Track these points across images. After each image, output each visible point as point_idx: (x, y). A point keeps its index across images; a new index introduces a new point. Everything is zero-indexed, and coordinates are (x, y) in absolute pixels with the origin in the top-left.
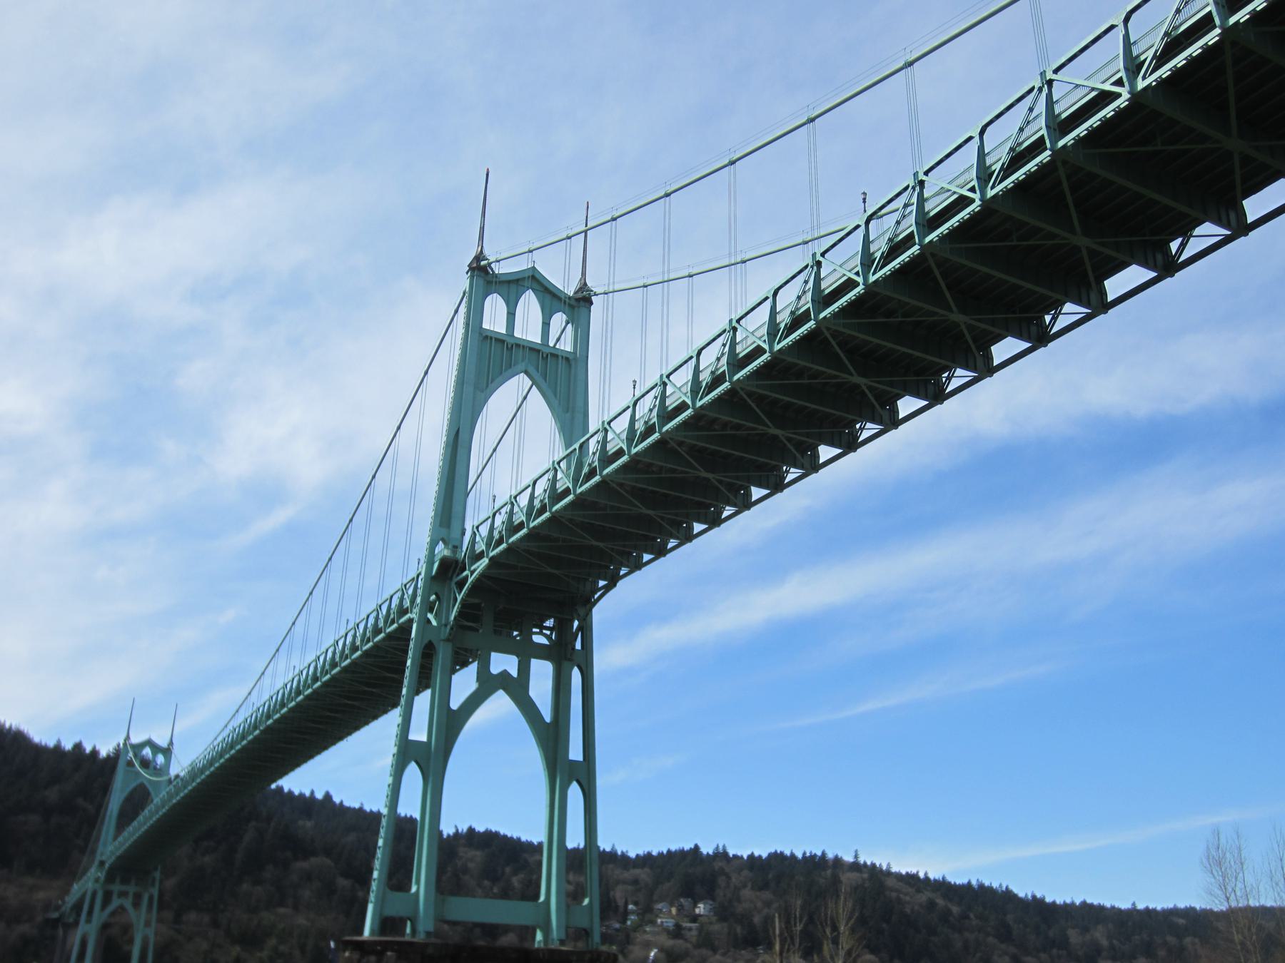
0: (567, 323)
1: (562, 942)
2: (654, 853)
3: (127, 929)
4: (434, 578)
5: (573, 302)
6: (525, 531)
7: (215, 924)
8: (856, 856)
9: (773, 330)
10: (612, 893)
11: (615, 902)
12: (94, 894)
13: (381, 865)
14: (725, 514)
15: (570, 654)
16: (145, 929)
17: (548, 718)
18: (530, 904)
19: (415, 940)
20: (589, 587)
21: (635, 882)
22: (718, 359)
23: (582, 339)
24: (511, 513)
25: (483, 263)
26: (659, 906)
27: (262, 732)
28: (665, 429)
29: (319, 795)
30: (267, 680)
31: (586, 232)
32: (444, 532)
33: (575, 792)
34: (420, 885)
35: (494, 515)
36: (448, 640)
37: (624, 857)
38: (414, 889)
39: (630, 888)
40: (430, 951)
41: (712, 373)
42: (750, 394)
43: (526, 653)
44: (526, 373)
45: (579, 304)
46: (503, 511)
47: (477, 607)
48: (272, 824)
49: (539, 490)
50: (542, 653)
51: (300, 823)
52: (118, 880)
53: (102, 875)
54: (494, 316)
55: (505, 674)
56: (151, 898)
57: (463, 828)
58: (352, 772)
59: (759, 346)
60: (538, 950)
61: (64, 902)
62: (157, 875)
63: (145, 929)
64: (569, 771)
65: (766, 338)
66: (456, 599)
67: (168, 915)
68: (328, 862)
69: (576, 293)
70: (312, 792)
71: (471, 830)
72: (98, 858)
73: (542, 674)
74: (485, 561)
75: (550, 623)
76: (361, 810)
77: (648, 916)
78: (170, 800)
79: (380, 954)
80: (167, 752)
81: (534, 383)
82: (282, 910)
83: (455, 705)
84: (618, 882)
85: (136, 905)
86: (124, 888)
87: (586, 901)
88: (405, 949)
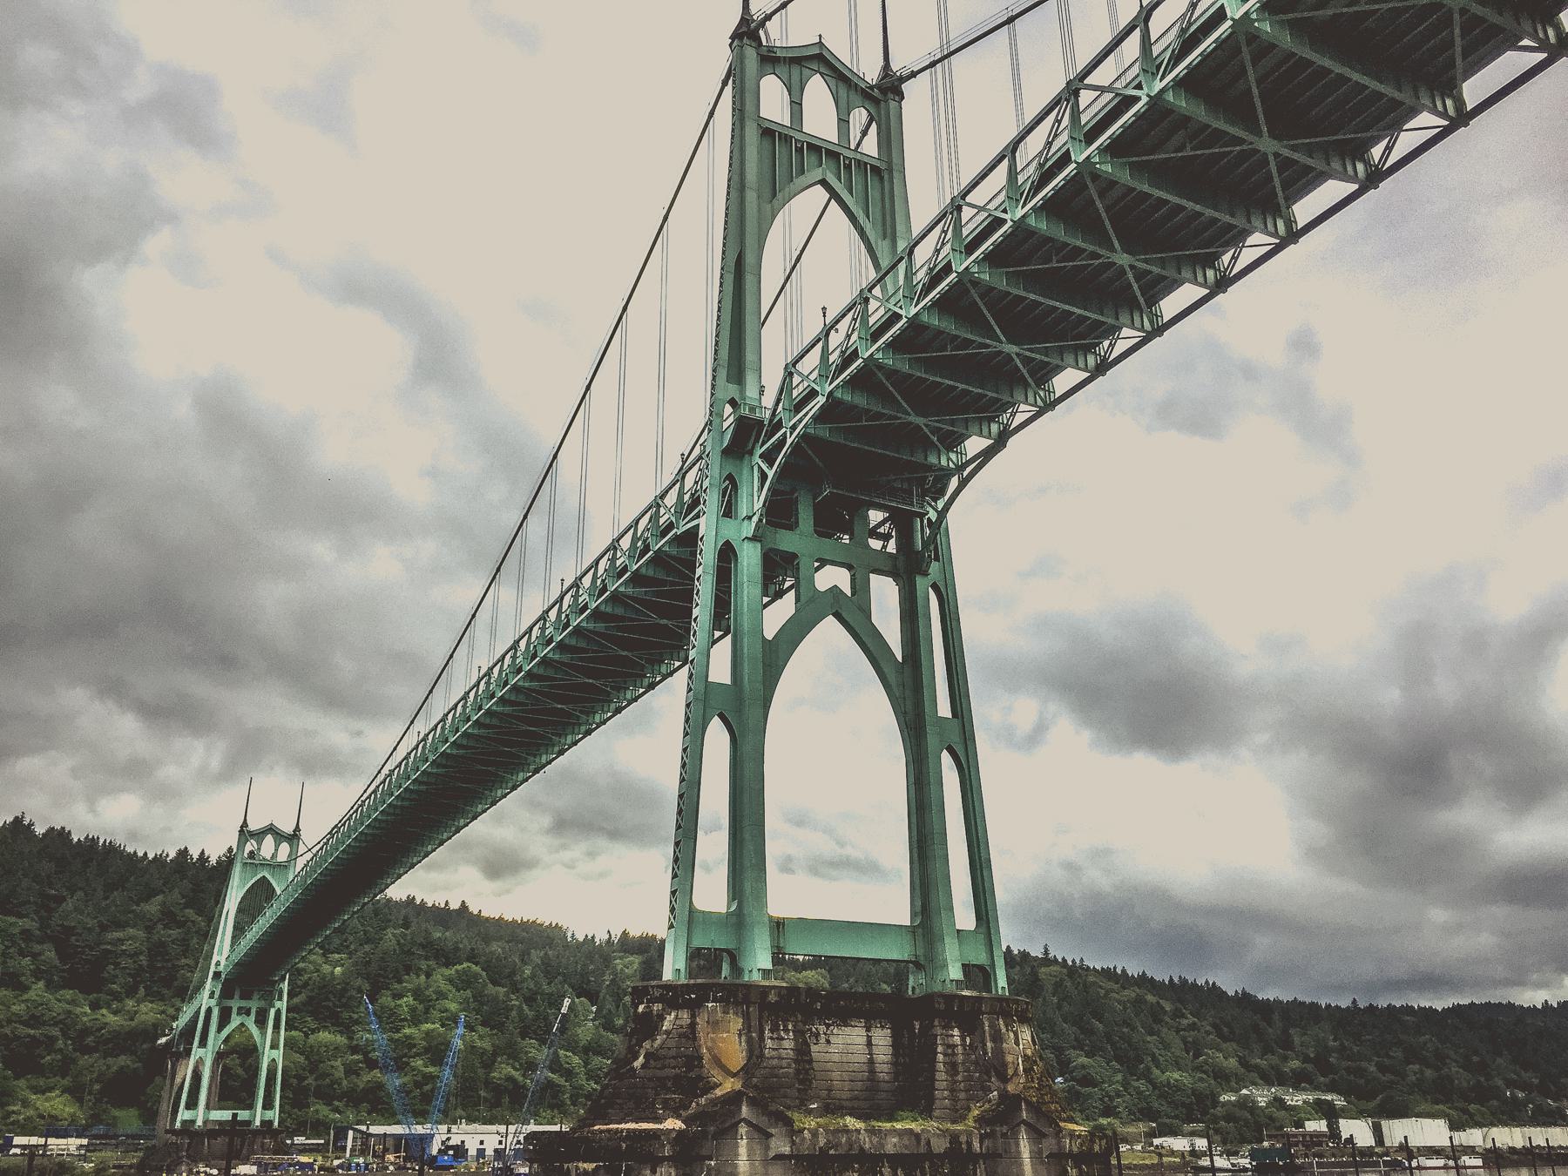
5: (876, 92)
8: (1046, 952)
12: (209, 1011)
15: (918, 561)
29: (455, 905)
32: (732, 391)
45: (884, 94)
55: (835, 590)
68: (477, 969)
73: (885, 594)
76: (501, 918)
80: (294, 838)
85: (261, 1021)
86: (244, 1004)
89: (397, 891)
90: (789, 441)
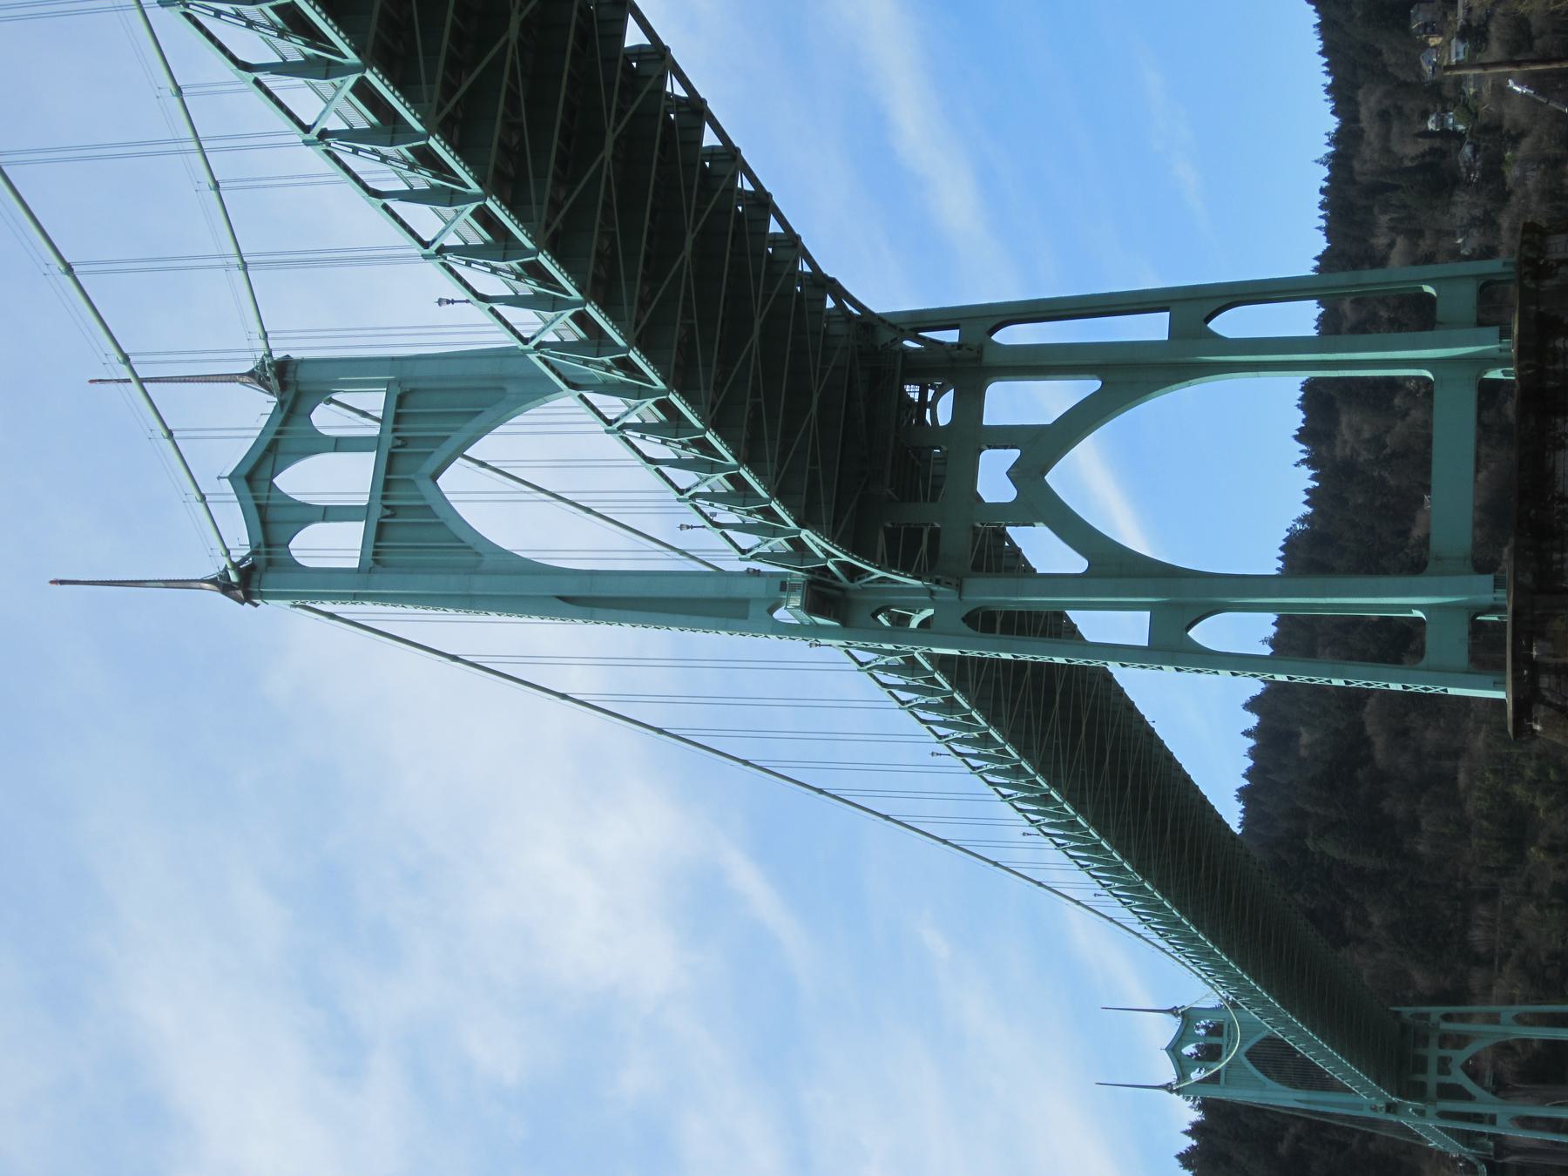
0: (331, 401)
1: (1505, 334)
2: (1329, 80)
3: (1505, 1048)
4: (844, 624)
5: (289, 395)
6: (744, 472)
7: (1489, 895)
9: (318, 69)
10: (1408, 163)
11: (1423, 155)
12: (1444, 1115)
13: (1377, 678)
14: (680, 91)
15: (971, 350)
16: (1505, 1021)
17: (1094, 385)
18: (1437, 395)
19: (1510, 608)
20: (838, 329)
21: (1384, 116)
22: (384, 159)
23: (357, 371)
24: (712, 497)
25: (234, 577)
26: (1428, 68)
27: (1146, 877)
28: (529, 244)
30: (1053, 877)
31: (141, 381)
33: (1230, 324)
34: (1409, 601)
35: (717, 525)
36: (959, 588)
37: (1338, 139)
38: (1418, 614)
39: (1396, 128)
40: (1528, 579)
41: (412, 168)
42: (449, 90)
43: (972, 435)
44: (435, 477)
45: (292, 384)
46: (708, 510)
47: (892, 536)
48: (1308, 808)
49: (666, 453)
50: (970, 404)
51: (1303, 753)
52: (1420, 1078)
53: (1411, 1105)
54: (332, 546)
55: (1015, 474)
56: (1447, 1017)
57: (1298, 451)
58: (1206, 727)
59: (354, 90)
60: (1520, 378)
61: (1460, 1159)
62: (1407, 1011)
63: (1505, 1021)
64: (1191, 336)
65: (337, 81)
66: (882, 580)
67: (1476, 978)
69: (271, 393)
70: (1247, 733)
71: (1302, 436)
72: (1381, 1115)
73: (1012, 403)
74: (805, 535)
75: (913, 392)
77: (1447, 91)
78: (1276, 1013)
79: (1534, 666)
80: (1188, 1017)
81: (459, 453)
82: (1462, 778)
83: (1076, 564)
84: (1386, 150)
85: (1461, 1041)
86: (1433, 1066)
87: (1428, 289)
88: (1528, 625)
89: (1232, 815)
90: (845, 558)
